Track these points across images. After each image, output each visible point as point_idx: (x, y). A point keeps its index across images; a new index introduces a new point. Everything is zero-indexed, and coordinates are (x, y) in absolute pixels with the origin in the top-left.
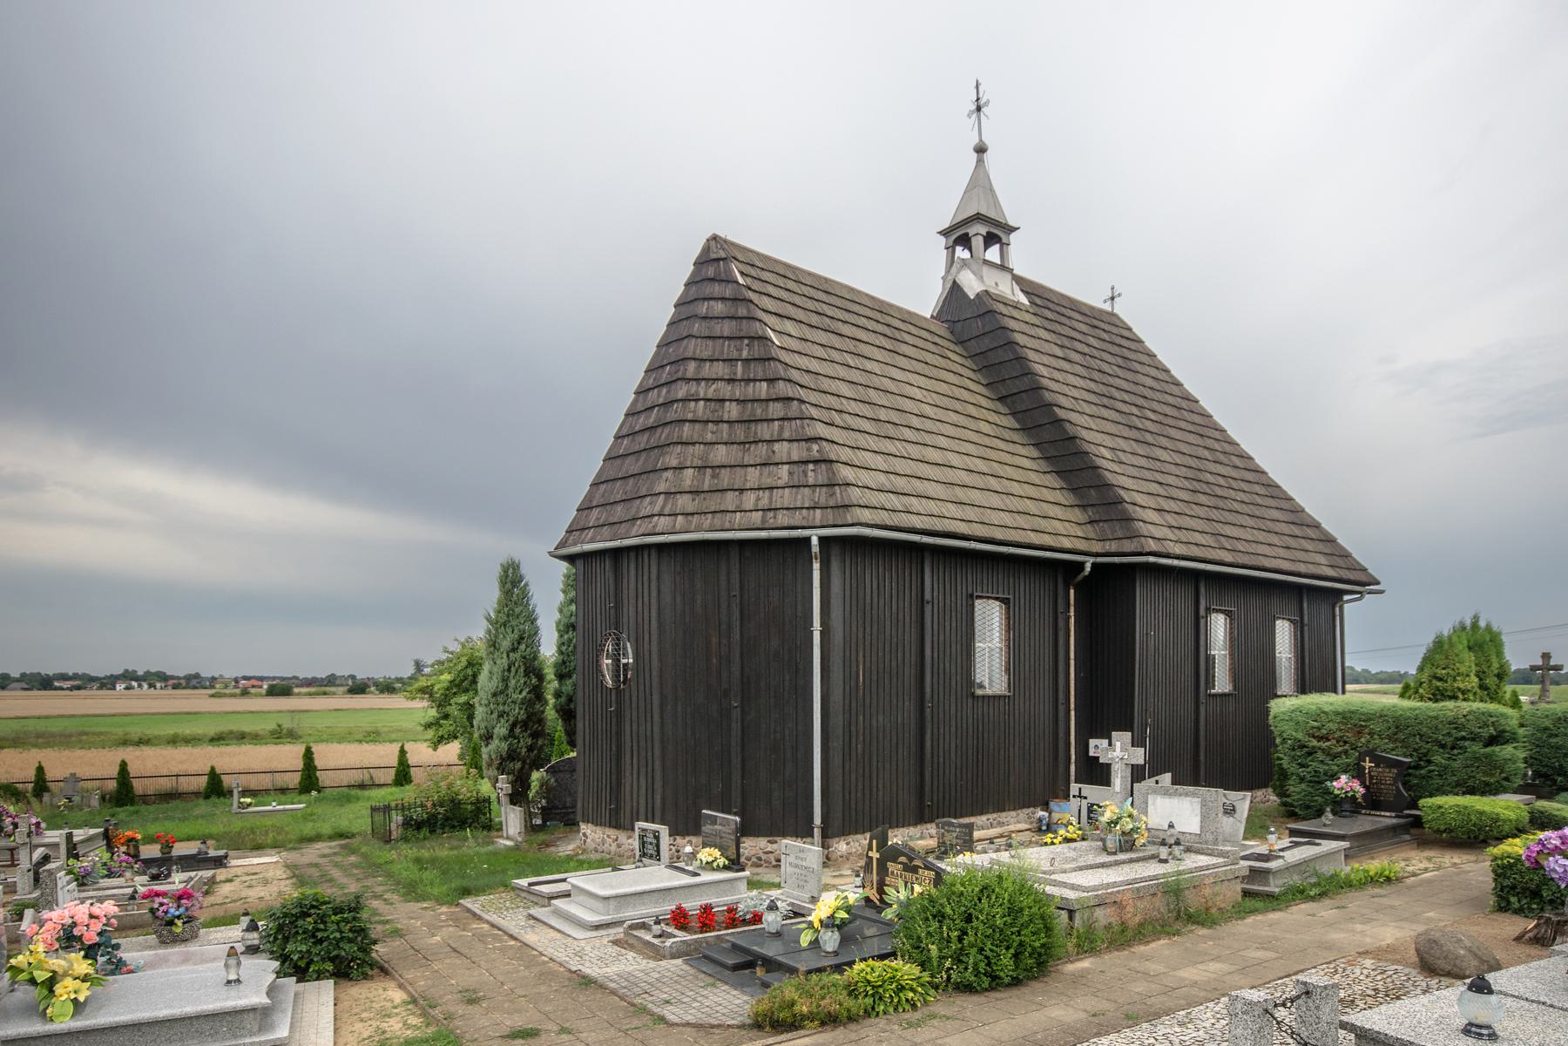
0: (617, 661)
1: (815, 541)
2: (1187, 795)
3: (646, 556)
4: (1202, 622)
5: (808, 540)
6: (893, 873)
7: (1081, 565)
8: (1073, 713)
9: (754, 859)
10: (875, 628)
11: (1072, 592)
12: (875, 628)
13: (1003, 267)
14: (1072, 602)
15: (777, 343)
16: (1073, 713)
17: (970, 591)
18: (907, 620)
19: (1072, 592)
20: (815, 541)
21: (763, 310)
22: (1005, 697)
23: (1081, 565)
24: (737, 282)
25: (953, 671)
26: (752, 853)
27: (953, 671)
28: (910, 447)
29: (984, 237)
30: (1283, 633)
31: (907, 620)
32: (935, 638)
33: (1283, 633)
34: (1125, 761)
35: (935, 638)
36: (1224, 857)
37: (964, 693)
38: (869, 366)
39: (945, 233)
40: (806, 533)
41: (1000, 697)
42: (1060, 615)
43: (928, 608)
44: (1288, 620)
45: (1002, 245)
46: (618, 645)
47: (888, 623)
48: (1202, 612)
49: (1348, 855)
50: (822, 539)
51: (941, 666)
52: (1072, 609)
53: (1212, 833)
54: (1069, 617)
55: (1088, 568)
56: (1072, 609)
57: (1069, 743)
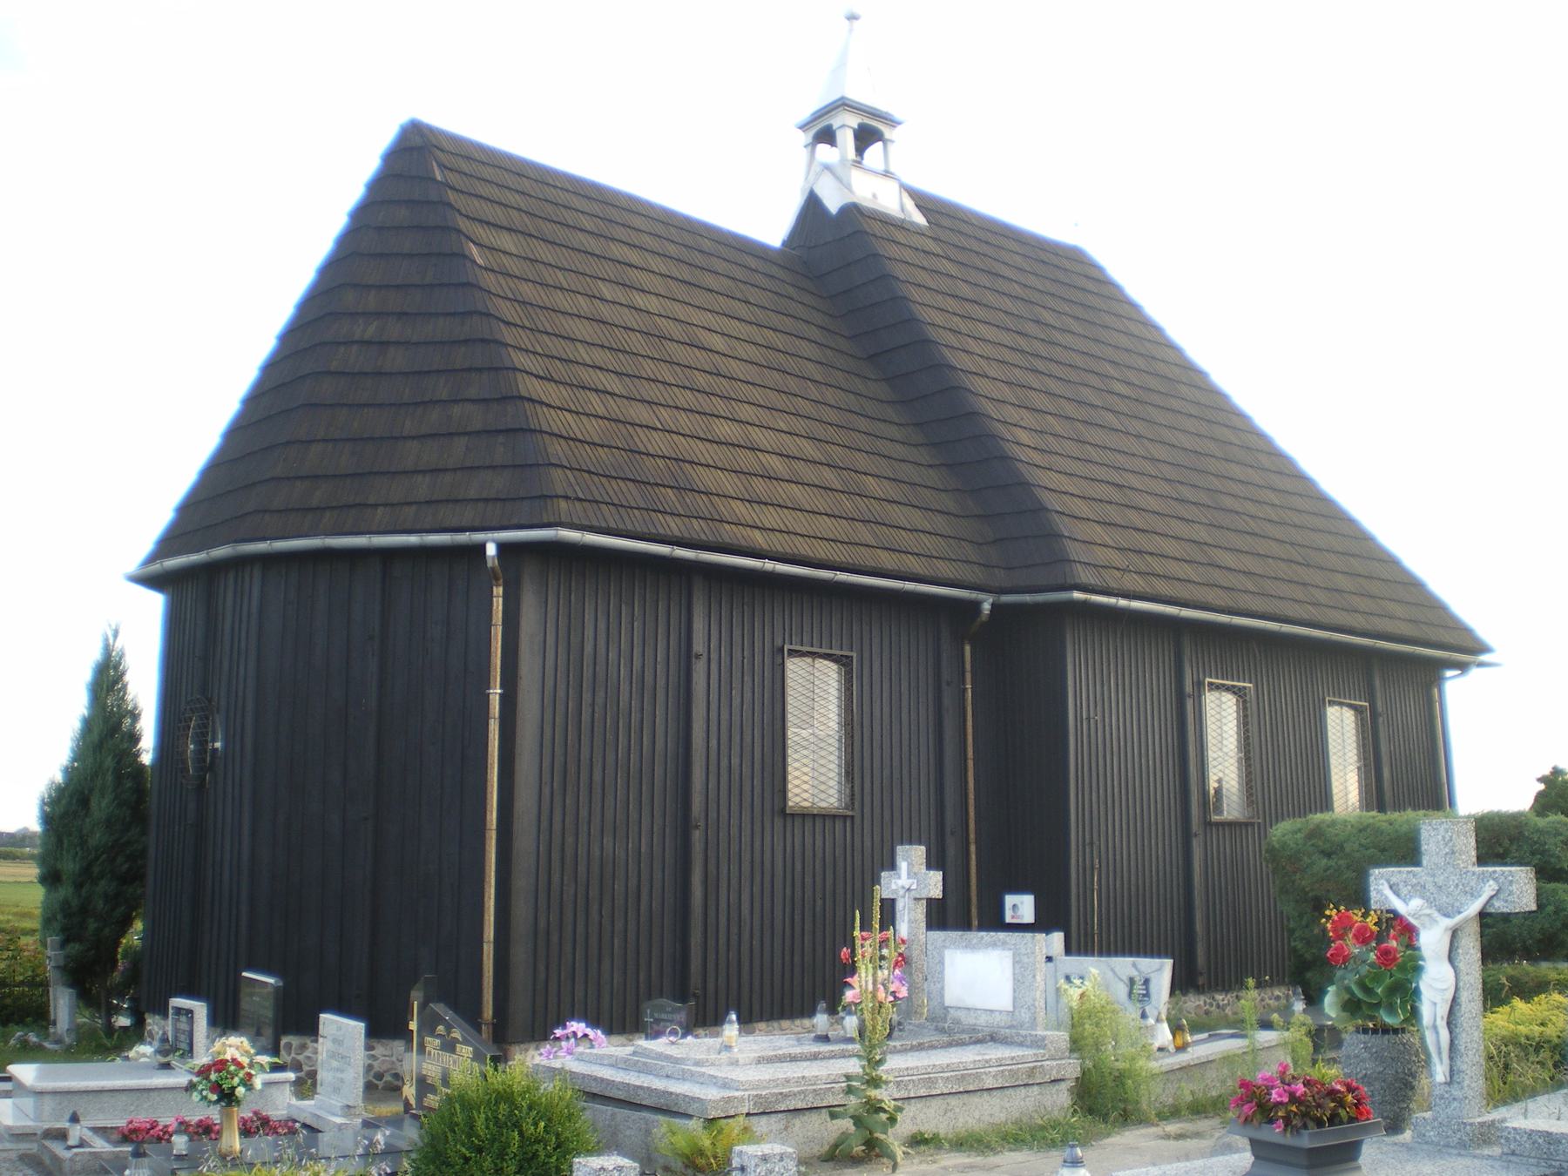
0: (202, 743)
1: (491, 550)
2: (994, 945)
3: (247, 579)
4: (1189, 704)
5: (481, 548)
6: (430, 1053)
7: (976, 605)
8: (973, 848)
9: (388, 1078)
10: (601, 694)
11: (968, 649)
12: (601, 694)
13: (887, 174)
14: (968, 666)
15: (480, 261)
16: (973, 848)
17: (778, 642)
18: (661, 682)
19: (968, 649)
20: (491, 550)
21: (468, 217)
22: (845, 817)
23: (976, 605)
24: (434, 180)
25: (746, 771)
26: (384, 1067)
27: (746, 771)
28: (682, 417)
29: (854, 130)
30: (1341, 725)
31: (661, 682)
32: (714, 715)
33: (1341, 725)
34: (914, 894)
35: (714, 715)
36: (1039, 1047)
37: (768, 806)
38: (640, 300)
39: (804, 127)
40: (478, 537)
41: (834, 817)
42: (944, 686)
43: (699, 668)
44: (1351, 706)
45: (885, 142)
46: (205, 726)
47: (624, 687)
48: (1188, 688)
49: (1504, 1120)
50: (503, 547)
51: (724, 763)
52: (968, 676)
53: (1029, 1009)
54: (965, 690)
55: (986, 607)
56: (968, 676)
57: (969, 900)
